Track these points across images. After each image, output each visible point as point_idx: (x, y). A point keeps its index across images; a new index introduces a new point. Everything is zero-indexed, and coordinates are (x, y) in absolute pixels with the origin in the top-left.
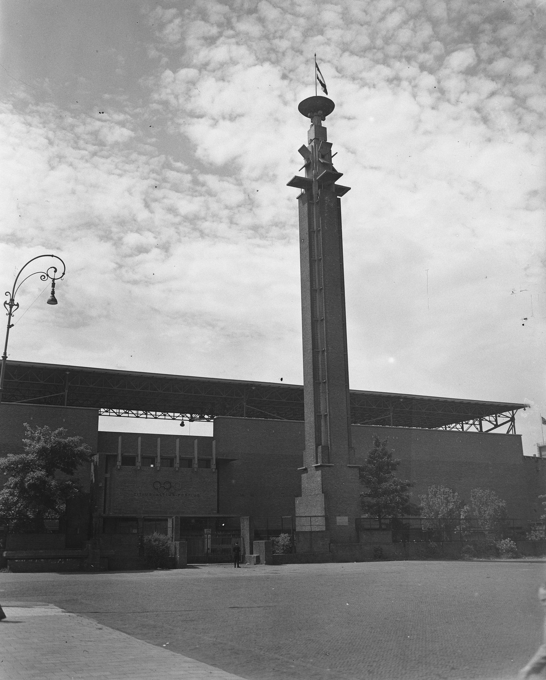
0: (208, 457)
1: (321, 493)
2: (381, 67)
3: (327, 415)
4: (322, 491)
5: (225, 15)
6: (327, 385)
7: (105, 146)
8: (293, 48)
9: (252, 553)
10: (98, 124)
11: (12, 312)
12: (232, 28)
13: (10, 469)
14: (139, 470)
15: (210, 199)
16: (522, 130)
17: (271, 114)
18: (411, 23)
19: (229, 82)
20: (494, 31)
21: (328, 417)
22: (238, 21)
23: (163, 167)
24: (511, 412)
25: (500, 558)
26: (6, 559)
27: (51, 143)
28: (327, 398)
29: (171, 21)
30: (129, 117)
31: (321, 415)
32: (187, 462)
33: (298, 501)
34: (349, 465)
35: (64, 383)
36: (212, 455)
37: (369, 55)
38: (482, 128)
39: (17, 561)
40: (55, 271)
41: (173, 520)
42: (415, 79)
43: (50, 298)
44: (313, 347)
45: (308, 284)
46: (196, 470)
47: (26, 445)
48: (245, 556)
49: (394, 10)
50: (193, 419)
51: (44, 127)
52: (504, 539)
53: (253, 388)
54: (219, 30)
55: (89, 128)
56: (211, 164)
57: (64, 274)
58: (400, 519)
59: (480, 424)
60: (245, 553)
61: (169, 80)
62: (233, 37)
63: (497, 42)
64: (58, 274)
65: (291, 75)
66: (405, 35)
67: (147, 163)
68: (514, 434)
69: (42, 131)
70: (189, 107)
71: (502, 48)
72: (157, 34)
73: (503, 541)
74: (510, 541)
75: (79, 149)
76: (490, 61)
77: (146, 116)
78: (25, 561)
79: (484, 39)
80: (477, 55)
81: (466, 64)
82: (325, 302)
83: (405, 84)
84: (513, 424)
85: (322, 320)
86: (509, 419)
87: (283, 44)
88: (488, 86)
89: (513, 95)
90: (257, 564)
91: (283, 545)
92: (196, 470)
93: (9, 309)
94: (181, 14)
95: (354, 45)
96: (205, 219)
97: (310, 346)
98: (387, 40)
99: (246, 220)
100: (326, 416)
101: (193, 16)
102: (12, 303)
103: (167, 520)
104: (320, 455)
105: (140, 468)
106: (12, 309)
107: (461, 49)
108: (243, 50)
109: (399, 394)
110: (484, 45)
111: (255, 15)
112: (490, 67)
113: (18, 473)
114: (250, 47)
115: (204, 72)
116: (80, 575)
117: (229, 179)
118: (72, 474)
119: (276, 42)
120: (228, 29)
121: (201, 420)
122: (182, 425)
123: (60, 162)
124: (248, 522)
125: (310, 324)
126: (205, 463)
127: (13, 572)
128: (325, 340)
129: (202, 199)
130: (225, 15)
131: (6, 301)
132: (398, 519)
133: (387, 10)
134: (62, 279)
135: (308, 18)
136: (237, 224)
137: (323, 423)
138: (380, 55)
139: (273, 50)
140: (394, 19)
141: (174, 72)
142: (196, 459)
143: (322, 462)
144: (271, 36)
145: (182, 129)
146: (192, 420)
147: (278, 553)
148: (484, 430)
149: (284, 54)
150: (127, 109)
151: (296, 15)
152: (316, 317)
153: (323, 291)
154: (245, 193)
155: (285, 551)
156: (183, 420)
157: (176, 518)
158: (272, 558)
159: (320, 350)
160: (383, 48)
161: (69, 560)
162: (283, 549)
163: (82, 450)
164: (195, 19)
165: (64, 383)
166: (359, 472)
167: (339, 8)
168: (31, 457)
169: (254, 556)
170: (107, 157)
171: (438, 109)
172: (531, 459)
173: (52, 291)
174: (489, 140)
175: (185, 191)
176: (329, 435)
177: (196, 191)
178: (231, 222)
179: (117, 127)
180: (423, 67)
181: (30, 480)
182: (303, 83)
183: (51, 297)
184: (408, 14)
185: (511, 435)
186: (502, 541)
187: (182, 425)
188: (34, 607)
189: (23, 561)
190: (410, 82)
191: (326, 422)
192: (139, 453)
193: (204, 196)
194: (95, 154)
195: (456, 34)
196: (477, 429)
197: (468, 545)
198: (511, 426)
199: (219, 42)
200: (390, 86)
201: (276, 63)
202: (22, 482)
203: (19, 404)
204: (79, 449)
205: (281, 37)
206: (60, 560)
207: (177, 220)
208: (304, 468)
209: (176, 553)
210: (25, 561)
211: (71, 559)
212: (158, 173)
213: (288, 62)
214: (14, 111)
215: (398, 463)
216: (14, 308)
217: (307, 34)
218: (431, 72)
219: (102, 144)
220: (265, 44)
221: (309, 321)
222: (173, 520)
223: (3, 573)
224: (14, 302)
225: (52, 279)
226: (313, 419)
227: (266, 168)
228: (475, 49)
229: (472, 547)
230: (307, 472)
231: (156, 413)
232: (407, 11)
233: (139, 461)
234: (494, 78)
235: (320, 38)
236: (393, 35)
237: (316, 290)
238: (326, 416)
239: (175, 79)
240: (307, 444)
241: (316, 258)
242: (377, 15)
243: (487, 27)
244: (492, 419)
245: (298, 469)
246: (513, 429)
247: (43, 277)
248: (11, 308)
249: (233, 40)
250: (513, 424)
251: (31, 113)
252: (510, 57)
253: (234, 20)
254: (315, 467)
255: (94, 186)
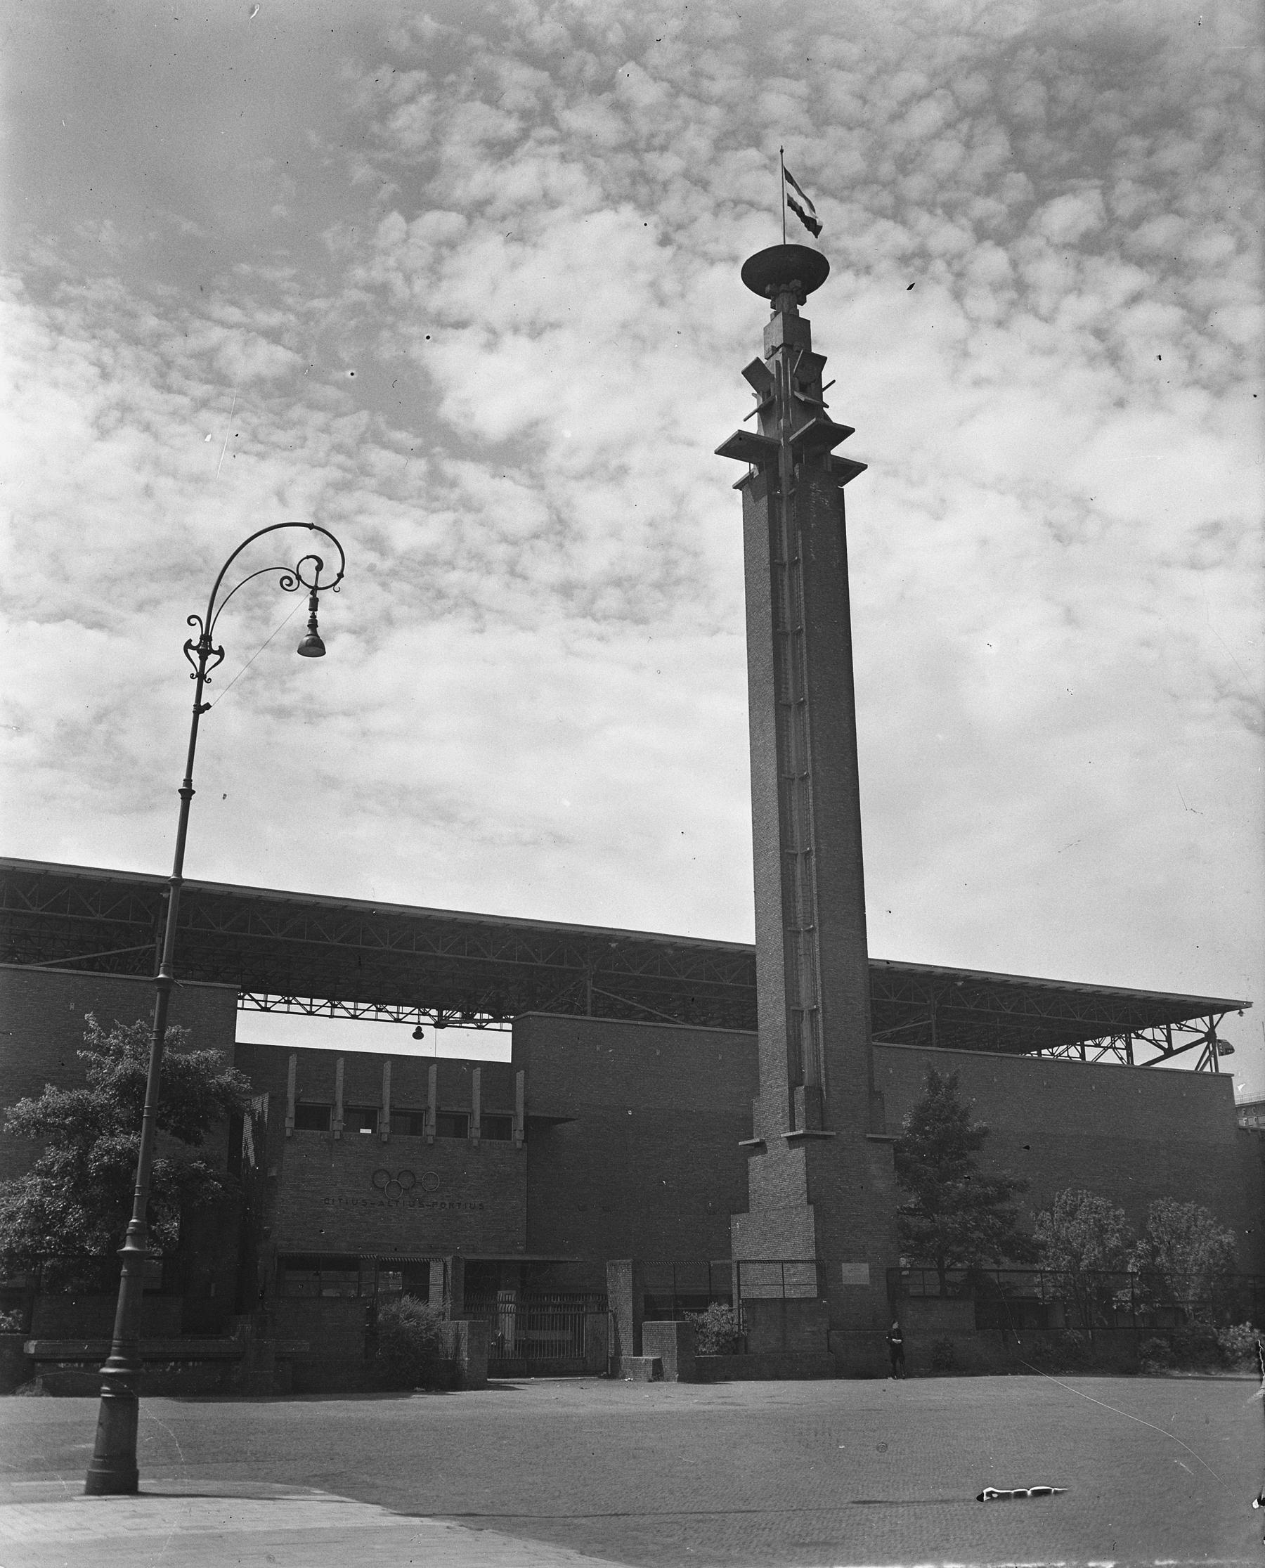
0: (504, 1112)
1: (805, 1202)
2: (884, 225)
3: (817, 1009)
4: (808, 1198)
5: (538, 91)
6: (817, 935)
7: (230, 386)
8: (686, 175)
9: (638, 1351)
10: (216, 334)
11: (206, 671)
12: (554, 123)
13: (41, 1128)
14: (337, 1140)
15: (468, 519)
16: (1195, 382)
17: (624, 326)
18: (964, 127)
19: (535, 245)
20: (1150, 152)
21: (820, 1016)
22: (568, 106)
23: (362, 440)
24: (1207, 1019)
25: (1231, 1371)
26: (33, 1359)
27: (105, 375)
28: (818, 971)
29: (411, 99)
30: (292, 317)
31: (803, 1011)
32: (455, 1124)
33: (738, 1223)
34: (871, 1136)
35: (153, 920)
36: (512, 1106)
37: (862, 197)
38: (1106, 376)
39: (62, 1365)
40: (319, 568)
41: (445, 1266)
42: (960, 256)
43: (308, 638)
44: (781, 844)
45: (770, 690)
46: (475, 1142)
47: (89, 1064)
48: (619, 1362)
49: (928, 95)
50: (443, 1022)
51: (94, 337)
52: (1237, 1324)
53: (613, 945)
54: (522, 125)
55: (194, 343)
56: (476, 436)
57: (341, 575)
58: (993, 1271)
59: (1129, 1048)
60: (618, 1352)
61: (396, 235)
62: (552, 141)
63: (1153, 179)
64: (327, 577)
65: (680, 237)
66: (946, 155)
67: (326, 430)
68: (1214, 1071)
69: (87, 347)
70: (436, 302)
71: (1164, 193)
72: (375, 128)
73: (1233, 1330)
74: (1251, 1329)
75: (169, 389)
76: (1137, 221)
77: (333, 316)
78: (82, 1365)
79: (1125, 172)
80: (1109, 210)
81: (1082, 227)
82: (812, 734)
83: (939, 266)
84: (1211, 1049)
85: (804, 779)
86: (1203, 1036)
87: (669, 164)
88: (1128, 279)
89: (1184, 303)
90: (655, 1380)
91: (718, 1334)
92: (475, 1142)
93: (198, 662)
94: (436, 85)
95: (828, 172)
96: (450, 565)
97: (775, 842)
98: (905, 164)
99: (547, 569)
100: (813, 1012)
101: (464, 89)
102: (205, 647)
103: (426, 1266)
104: (800, 1108)
105: (341, 1135)
106: (207, 662)
107: (1073, 191)
108: (574, 175)
109: (955, 969)
110: (1125, 186)
111: (607, 96)
112: (1133, 237)
113: (70, 1138)
114: (590, 170)
115: (479, 221)
116: (384, 1401)
117: (516, 473)
118: (198, 1142)
119: (651, 157)
120: (543, 125)
121: (463, 1025)
122: (418, 1035)
123: (121, 420)
124: (630, 1275)
125: (775, 788)
126: (497, 1127)
127: (54, 1395)
128: (812, 825)
129: (449, 516)
130: (538, 91)
131: (190, 640)
132: (986, 1270)
133: (914, 94)
134: (336, 588)
135: (731, 108)
136: (525, 578)
137: (806, 1032)
138: (886, 199)
139: (641, 176)
140: (928, 116)
141: (410, 218)
142: (478, 1117)
143: (808, 1128)
144: (642, 145)
145: (414, 351)
146: (439, 1024)
147: (704, 1353)
148: (1138, 1062)
149: (665, 186)
150: (290, 300)
151: (702, 99)
152: (790, 772)
153: (807, 708)
154: (550, 506)
155: (721, 1347)
156: (419, 1023)
157: (456, 1260)
158: (694, 1364)
159: (799, 850)
160: (894, 182)
161: (194, 1364)
162: (717, 1343)
163: (229, 1084)
164: (470, 97)
165: (153, 920)
166: (895, 1153)
167: (801, 88)
168: (99, 1097)
169: (646, 1360)
170: (234, 412)
171: (1008, 329)
172: (1249, 1134)
173: (310, 621)
174: (1120, 404)
175: (411, 497)
176: (822, 1059)
177: (437, 499)
178: (512, 573)
179: (262, 342)
180: (982, 233)
181: (102, 1156)
182: (705, 255)
183: (308, 635)
184: (958, 107)
185: (1206, 1074)
186: (1232, 1330)
187: (418, 1035)
188: (279, 1499)
189: (79, 1365)
190: (949, 264)
191: (813, 1028)
192: (339, 1097)
193: (455, 511)
194: (204, 404)
195: (1064, 158)
196: (1121, 1059)
197: (1154, 1339)
198: (1207, 1054)
199: (519, 152)
200: (905, 271)
201: (647, 207)
202: (82, 1161)
203: (45, 969)
204: (221, 1081)
205: (663, 149)
206: (173, 1364)
207: (388, 564)
208: (757, 1140)
209: (457, 1349)
210: (82, 1365)
211: (201, 1363)
212: (349, 454)
213: (671, 206)
214: (26, 296)
215: (985, 1132)
216: (212, 659)
217: (723, 143)
218: (1002, 240)
219: (221, 380)
220: (627, 162)
221: (772, 781)
222: (445, 1266)
223: (28, 1396)
224: (210, 644)
225: (309, 587)
226: (781, 1019)
227: (603, 449)
228: (1104, 194)
229: (1164, 1343)
230: (765, 1152)
231: (356, 1006)
232: (957, 101)
233: (340, 1117)
234: (1142, 260)
235: (752, 154)
236: (918, 153)
237: (790, 707)
238: (813, 1012)
239: (408, 235)
240: (765, 1082)
241: (789, 628)
242: (887, 105)
243: (1138, 144)
244: (1159, 1035)
245: (740, 1143)
246: (1213, 1059)
247: (286, 582)
248: (203, 659)
249: (556, 149)
250: (1211, 1049)
251: (64, 303)
252: (1179, 213)
253: (558, 103)
254: (788, 1138)
255: (198, 479)
